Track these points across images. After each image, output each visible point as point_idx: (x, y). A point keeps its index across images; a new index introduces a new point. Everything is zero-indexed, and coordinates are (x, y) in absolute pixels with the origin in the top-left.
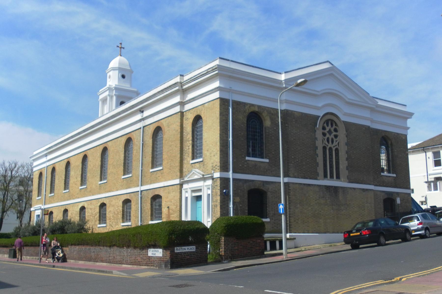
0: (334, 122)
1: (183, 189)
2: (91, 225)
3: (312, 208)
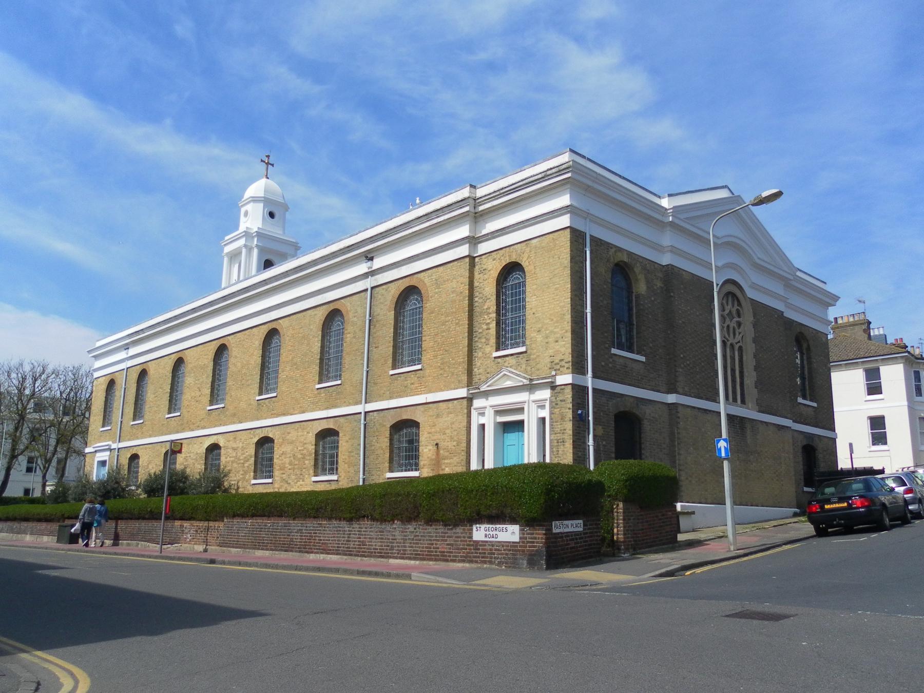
2: (235, 480)
3: (710, 456)
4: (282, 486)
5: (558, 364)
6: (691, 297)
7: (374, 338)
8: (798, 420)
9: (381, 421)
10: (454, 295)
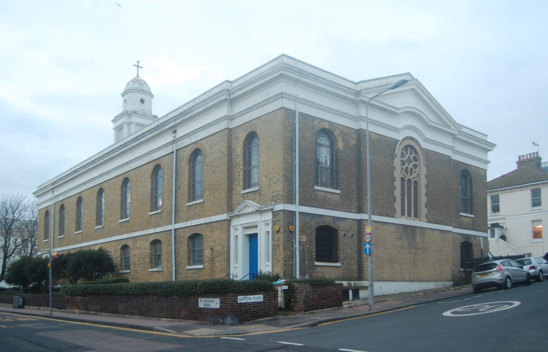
1: (231, 226)
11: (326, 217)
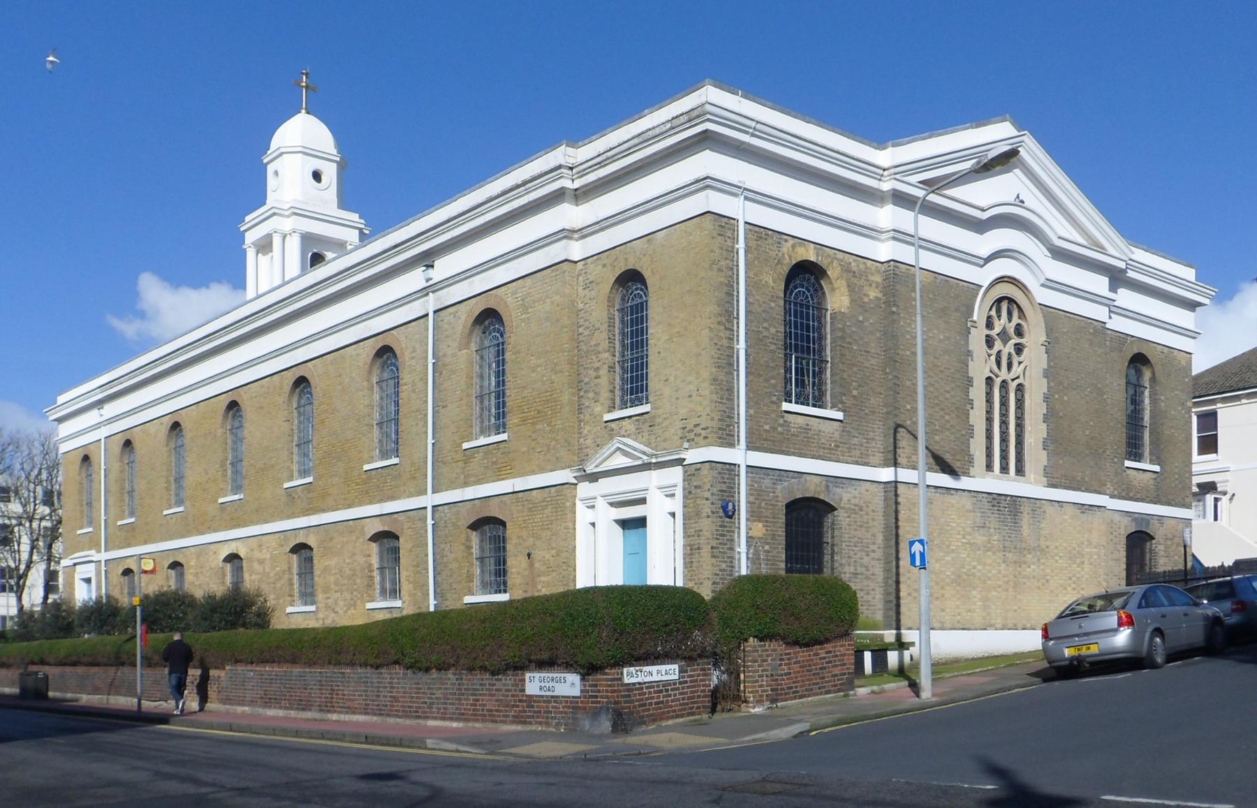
0: (1015, 306)
3: (953, 558)
4: (327, 616)
5: (692, 431)
6: (930, 311)
7: (440, 391)
8: (1123, 494)
9: (454, 520)
10: (548, 324)
11: (808, 478)
